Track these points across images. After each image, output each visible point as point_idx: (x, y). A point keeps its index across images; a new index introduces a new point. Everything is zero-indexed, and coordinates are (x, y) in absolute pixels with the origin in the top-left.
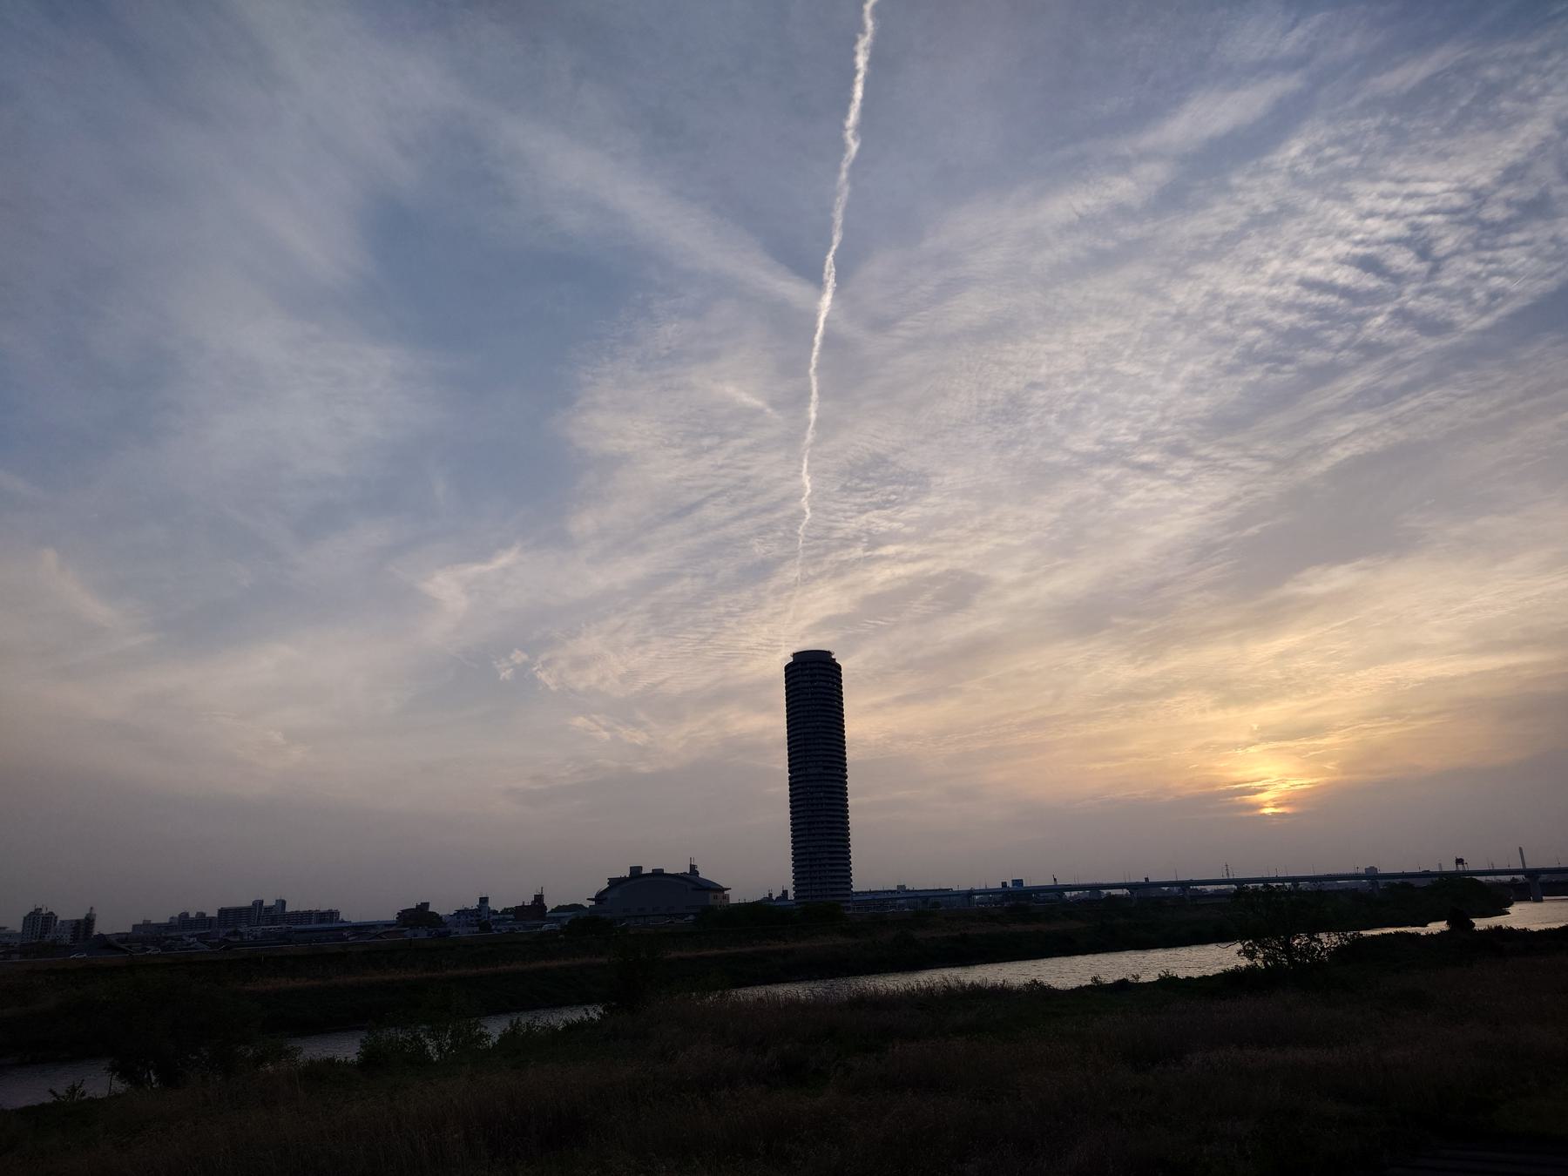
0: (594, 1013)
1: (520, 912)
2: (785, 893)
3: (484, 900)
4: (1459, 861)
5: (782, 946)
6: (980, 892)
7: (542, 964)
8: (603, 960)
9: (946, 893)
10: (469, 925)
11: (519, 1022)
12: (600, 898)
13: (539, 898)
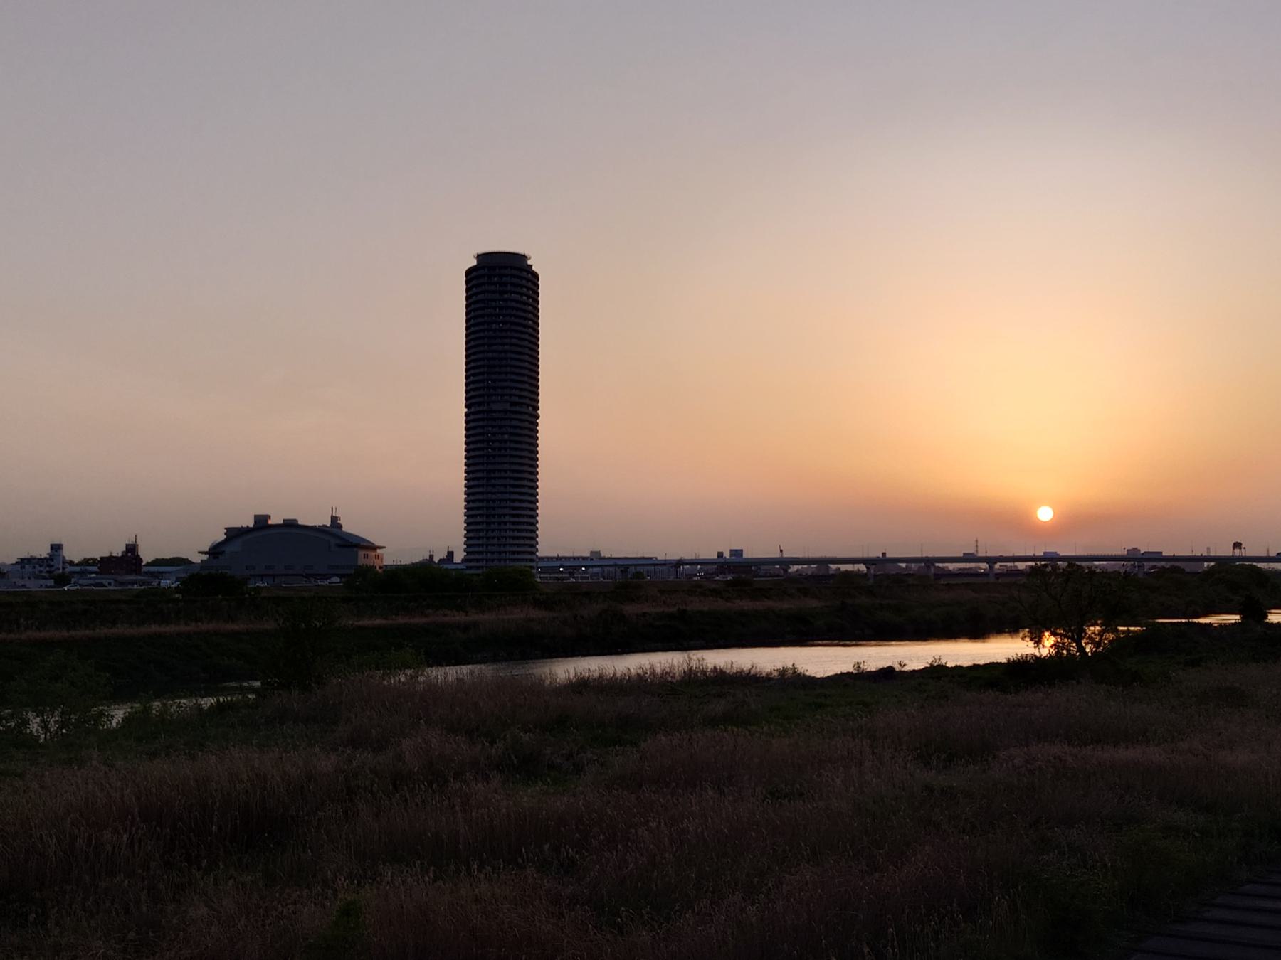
0: (1235, 618)
1: (107, 564)
2: (450, 554)
3: (56, 548)
4: (1237, 545)
5: (460, 617)
6: (693, 563)
7: (155, 628)
8: (269, 625)
9: (651, 562)
10: (37, 577)
11: (690, 659)
12: (215, 551)
13: (132, 549)
